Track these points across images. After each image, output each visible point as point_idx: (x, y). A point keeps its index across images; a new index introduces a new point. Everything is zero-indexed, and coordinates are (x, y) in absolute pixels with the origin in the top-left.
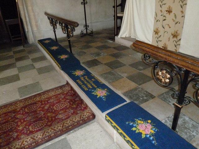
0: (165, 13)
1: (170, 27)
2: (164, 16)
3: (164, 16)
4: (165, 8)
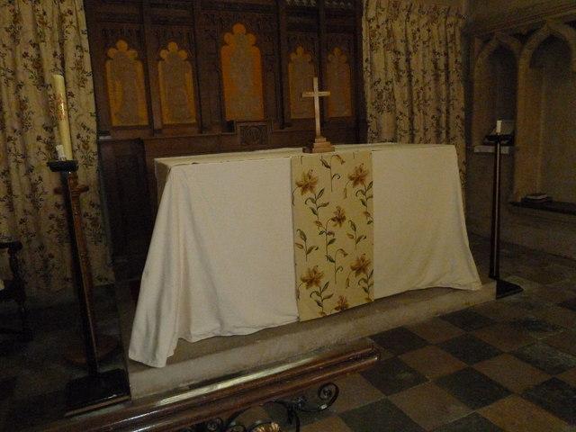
0: (331, 226)
1: (343, 162)
2: (330, 233)
3: (330, 233)
4: (326, 215)
